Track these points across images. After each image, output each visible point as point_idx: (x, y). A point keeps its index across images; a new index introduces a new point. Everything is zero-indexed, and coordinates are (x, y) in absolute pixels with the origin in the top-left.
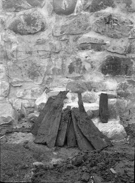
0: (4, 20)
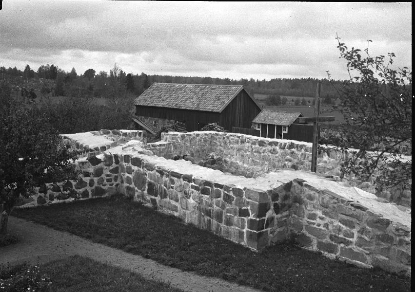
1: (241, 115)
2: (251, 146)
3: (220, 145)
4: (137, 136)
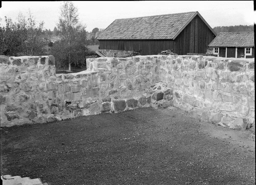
0: (248, 75)
1: (196, 42)
2: (216, 72)
3: (170, 73)
4: (39, 64)
